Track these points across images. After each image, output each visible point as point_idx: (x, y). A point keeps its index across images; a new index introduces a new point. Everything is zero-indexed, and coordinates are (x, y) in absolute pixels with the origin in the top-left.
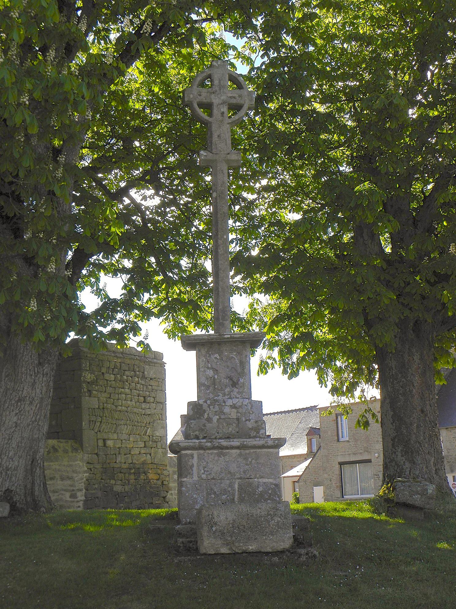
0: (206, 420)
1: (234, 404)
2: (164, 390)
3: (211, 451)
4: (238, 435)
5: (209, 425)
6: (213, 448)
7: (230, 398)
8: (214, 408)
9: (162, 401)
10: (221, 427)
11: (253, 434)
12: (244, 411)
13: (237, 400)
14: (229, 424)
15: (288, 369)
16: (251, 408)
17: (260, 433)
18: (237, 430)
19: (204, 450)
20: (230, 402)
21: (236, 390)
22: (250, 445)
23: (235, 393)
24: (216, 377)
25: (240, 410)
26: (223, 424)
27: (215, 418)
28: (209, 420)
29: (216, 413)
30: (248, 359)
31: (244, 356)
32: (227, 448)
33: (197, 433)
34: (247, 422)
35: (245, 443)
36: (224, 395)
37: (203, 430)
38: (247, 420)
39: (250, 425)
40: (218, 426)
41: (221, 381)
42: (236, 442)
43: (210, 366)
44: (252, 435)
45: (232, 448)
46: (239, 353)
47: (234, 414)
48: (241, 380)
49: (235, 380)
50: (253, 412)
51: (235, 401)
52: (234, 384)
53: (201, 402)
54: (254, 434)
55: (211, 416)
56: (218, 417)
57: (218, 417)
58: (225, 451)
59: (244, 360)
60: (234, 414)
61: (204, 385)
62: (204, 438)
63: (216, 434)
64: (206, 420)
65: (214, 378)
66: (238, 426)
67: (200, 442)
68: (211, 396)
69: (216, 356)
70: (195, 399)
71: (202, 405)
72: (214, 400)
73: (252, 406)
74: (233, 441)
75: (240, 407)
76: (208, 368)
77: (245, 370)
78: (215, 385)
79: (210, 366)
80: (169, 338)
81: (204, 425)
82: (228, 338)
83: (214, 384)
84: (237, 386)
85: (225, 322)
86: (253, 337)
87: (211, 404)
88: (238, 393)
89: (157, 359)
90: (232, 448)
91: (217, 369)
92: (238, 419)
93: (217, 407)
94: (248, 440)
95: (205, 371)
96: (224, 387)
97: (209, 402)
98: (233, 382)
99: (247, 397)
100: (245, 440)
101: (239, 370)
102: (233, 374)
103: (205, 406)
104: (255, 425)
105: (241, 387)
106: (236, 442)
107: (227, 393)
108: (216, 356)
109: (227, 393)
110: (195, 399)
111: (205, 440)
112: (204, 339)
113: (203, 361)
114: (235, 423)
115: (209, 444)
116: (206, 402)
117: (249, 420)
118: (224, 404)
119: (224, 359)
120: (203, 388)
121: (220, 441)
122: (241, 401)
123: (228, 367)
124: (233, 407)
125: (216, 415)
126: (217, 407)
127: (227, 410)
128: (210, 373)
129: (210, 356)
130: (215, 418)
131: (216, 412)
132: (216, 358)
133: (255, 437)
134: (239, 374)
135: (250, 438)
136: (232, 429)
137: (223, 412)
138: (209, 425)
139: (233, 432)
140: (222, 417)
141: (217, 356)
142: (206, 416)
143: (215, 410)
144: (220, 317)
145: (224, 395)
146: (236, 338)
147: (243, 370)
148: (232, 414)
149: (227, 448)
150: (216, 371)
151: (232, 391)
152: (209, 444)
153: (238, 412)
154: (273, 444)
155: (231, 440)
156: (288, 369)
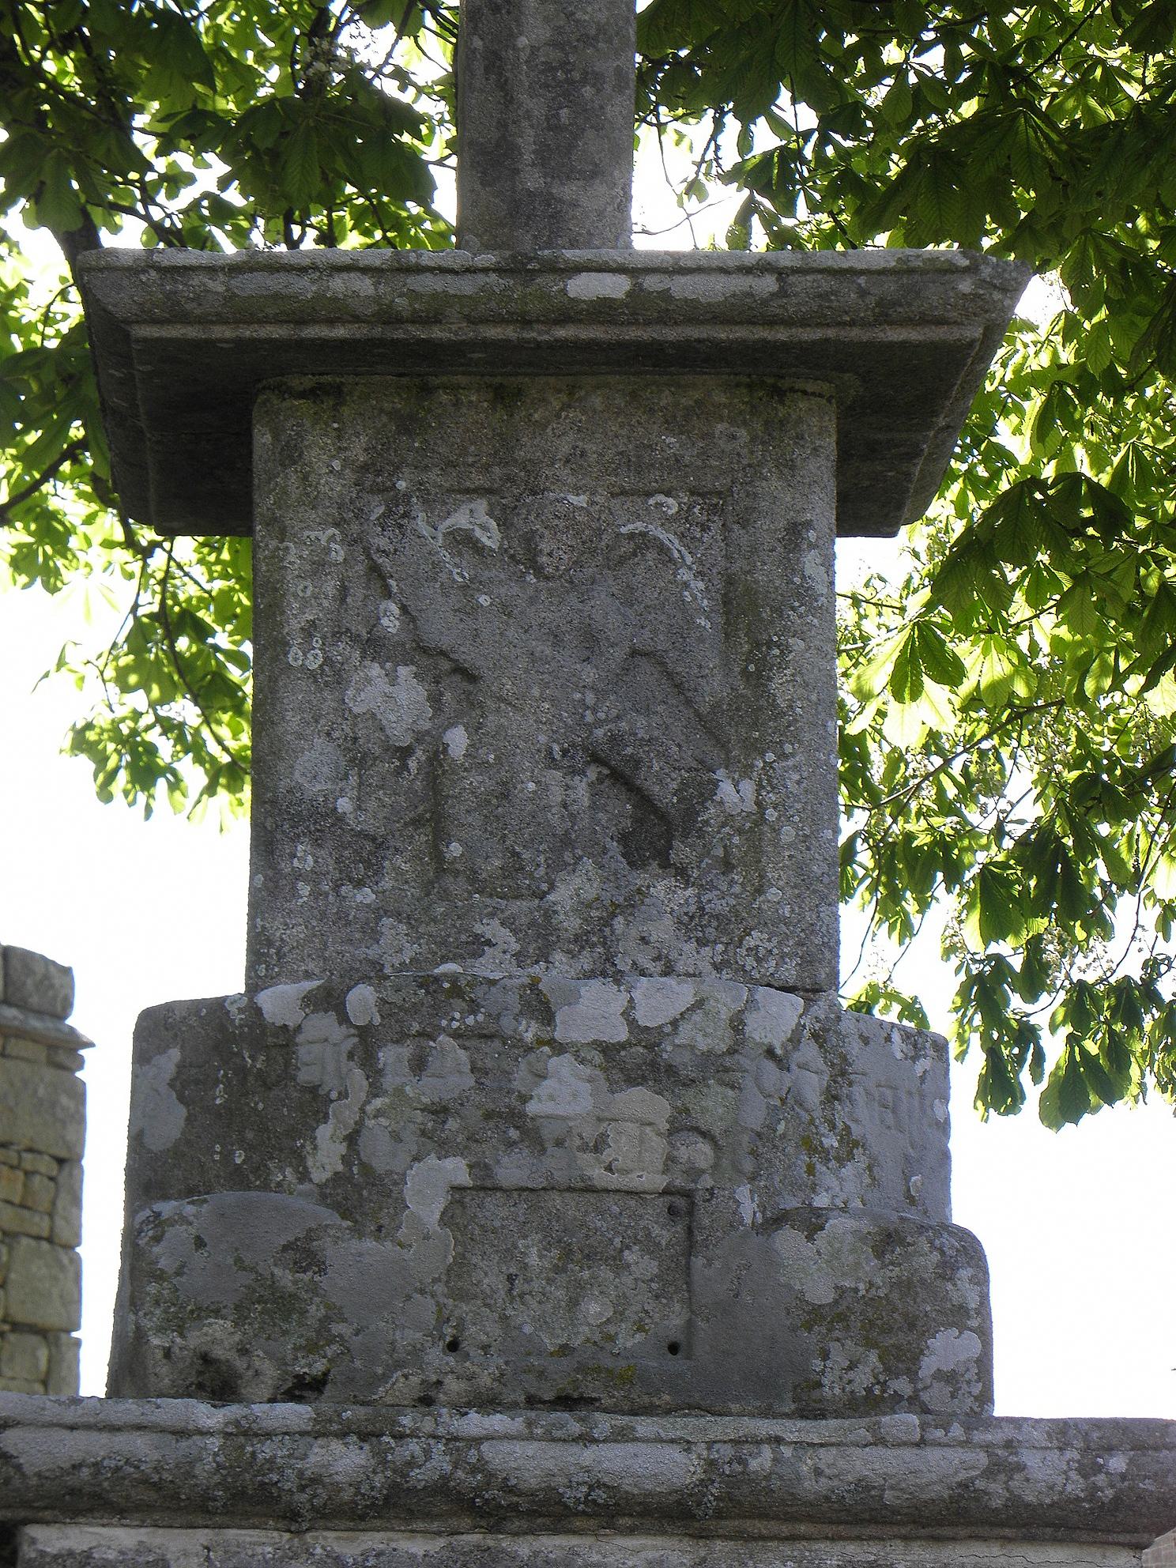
0: (324, 1194)
1: (648, 1038)
2: (64, 1234)
3: (373, 1540)
4: (675, 1380)
5: (352, 1256)
6: (395, 1504)
7: (607, 970)
8: (419, 1065)
9: (49, 1316)
10: (490, 1277)
11: (846, 1368)
12: (755, 1116)
13: (683, 994)
14: (577, 1254)
15: (1025, 1076)
16: (831, 1097)
17: (929, 1365)
18: (674, 1320)
19: (290, 1518)
20: (595, 1011)
21: (667, 894)
22: (811, 1487)
23: (663, 930)
24: (458, 740)
25: (712, 1104)
26: (509, 1254)
27: (429, 1184)
28: (363, 1196)
29: (437, 1126)
30: (810, 561)
31: (768, 528)
32: (550, 1511)
33: (219, 1335)
34: (789, 1240)
35: (761, 1461)
36: (542, 939)
37: (284, 1305)
38: (777, 1221)
39: (812, 1269)
40: (459, 1268)
41: (505, 794)
42: (653, 1456)
43: (391, 622)
44: (832, 1389)
45: (614, 1510)
46: (719, 503)
47: (636, 1144)
48: (734, 794)
49: (665, 791)
50: (851, 1145)
51: (659, 1001)
52: (655, 833)
53: (281, 1002)
54: (862, 1378)
55: (379, 1151)
56: (457, 1169)
57: (457, 1169)
58: (523, 1548)
59: (766, 574)
60: (636, 1144)
61: (319, 822)
62: (301, 1389)
63: (435, 1356)
64: (324, 1194)
65: (438, 755)
66: (678, 1272)
67: (241, 1432)
68: (397, 945)
69: (460, 519)
70: (225, 977)
71: (285, 1038)
72: (429, 983)
73: (841, 1071)
74: (622, 1436)
75: (719, 1067)
76: (374, 646)
77: (780, 687)
78: (440, 837)
79: (391, 622)
80: (105, 795)
81: (304, 1255)
82: (602, 310)
83: (434, 820)
84: (682, 852)
85: (568, 191)
86: (884, 315)
87: (397, 1019)
88: (693, 924)
89: (23, 1006)
90: (614, 1510)
91: (467, 655)
92: (682, 1204)
93: (452, 1056)
94: (793, 1430)
95: (334, 676)
96: (536, 860)
97: (362, 999)
98: (644, 801)
99: (790, 972)
100: (765, 1427)
101: (715, 685)
102: (641, 724)
103: (322, 1048)
104: (872, 1275)
105: (727, 866)
106: (653, 1456)
107: (571, 924)
108: (460, 519)
109: (571, 924)
110: (225, 977)
111: (295, 1414)
112: (338, 311)
113: (319, 566)
114: (651, 1247)
115: (345, 1461)
116: (329, 1000)
117: (812, 1222)
118: (530, 1031)
119: (554, 550)
120: (305, 857)
121: (475, 1423)
122: (726, 997)
123: (591, 641)
124: (637, 1060)
125: (445, 1148)
126: (452, 1056)
127: (563, 1093)
128: (394, 698)
129: (397, 515)
130: (429, 1184)
131: (440, 1111)
132: (462, 541)
133: (869, 1404)
134: (708, 725)
135: (817, 1413)
136: (613, 1311)
137: (516, 1117)
138: (352, 1256)
139: (628, 1340)
140: (513, 1169)
141: (474, 517)
142: (327, 1153)
143: (427, 1089)
144: (527, 141)
145: (542, 939)
146: (694, 312)
147: (758, 679)
148: (620, 1149)
149: (550, 1511)
150: (454, 677)
151: (632, 903)
152: (345, 1461)
153: (681, 1126)
154: (1076, 1486)
155: (604, 1423)
156: (1025, 1076)
